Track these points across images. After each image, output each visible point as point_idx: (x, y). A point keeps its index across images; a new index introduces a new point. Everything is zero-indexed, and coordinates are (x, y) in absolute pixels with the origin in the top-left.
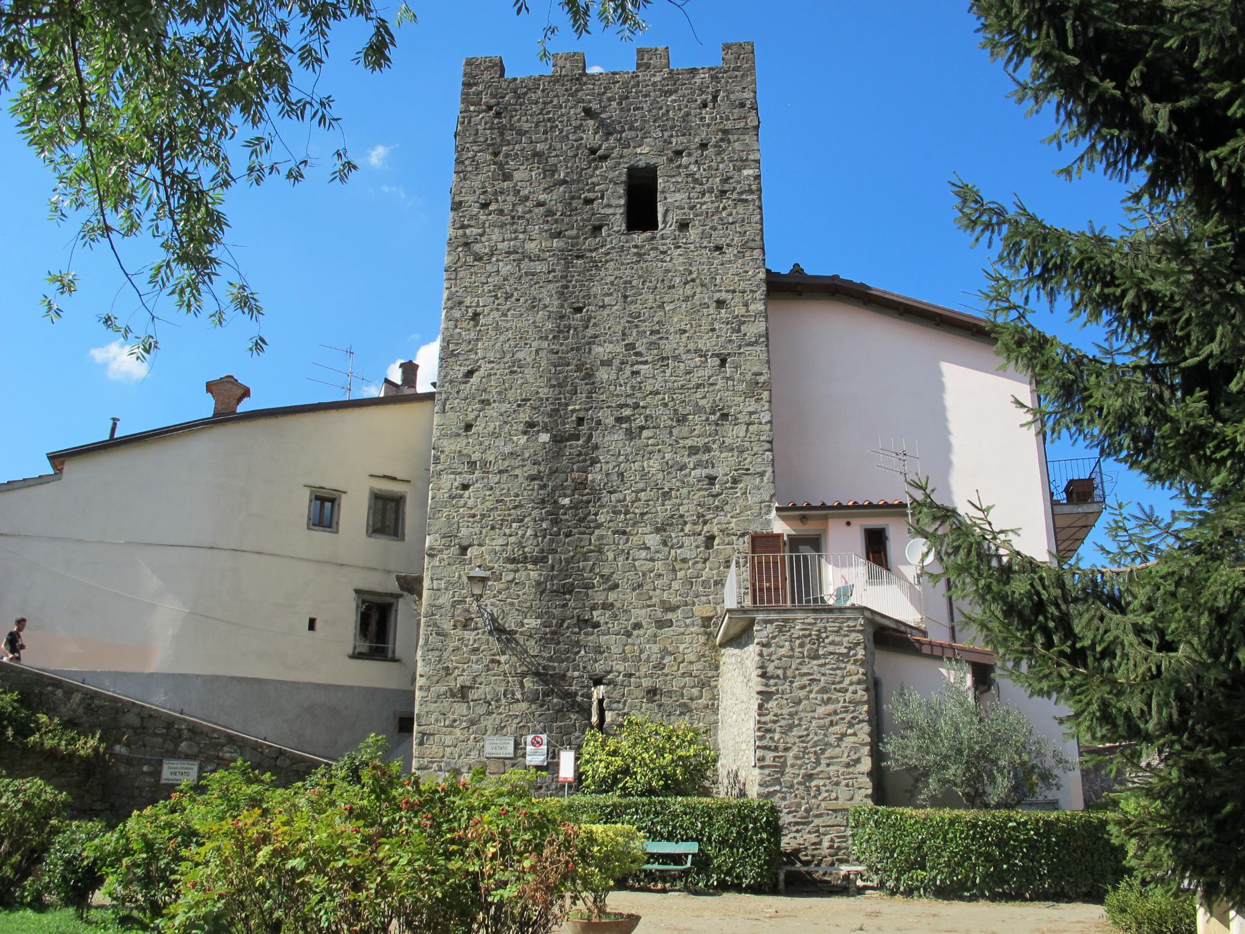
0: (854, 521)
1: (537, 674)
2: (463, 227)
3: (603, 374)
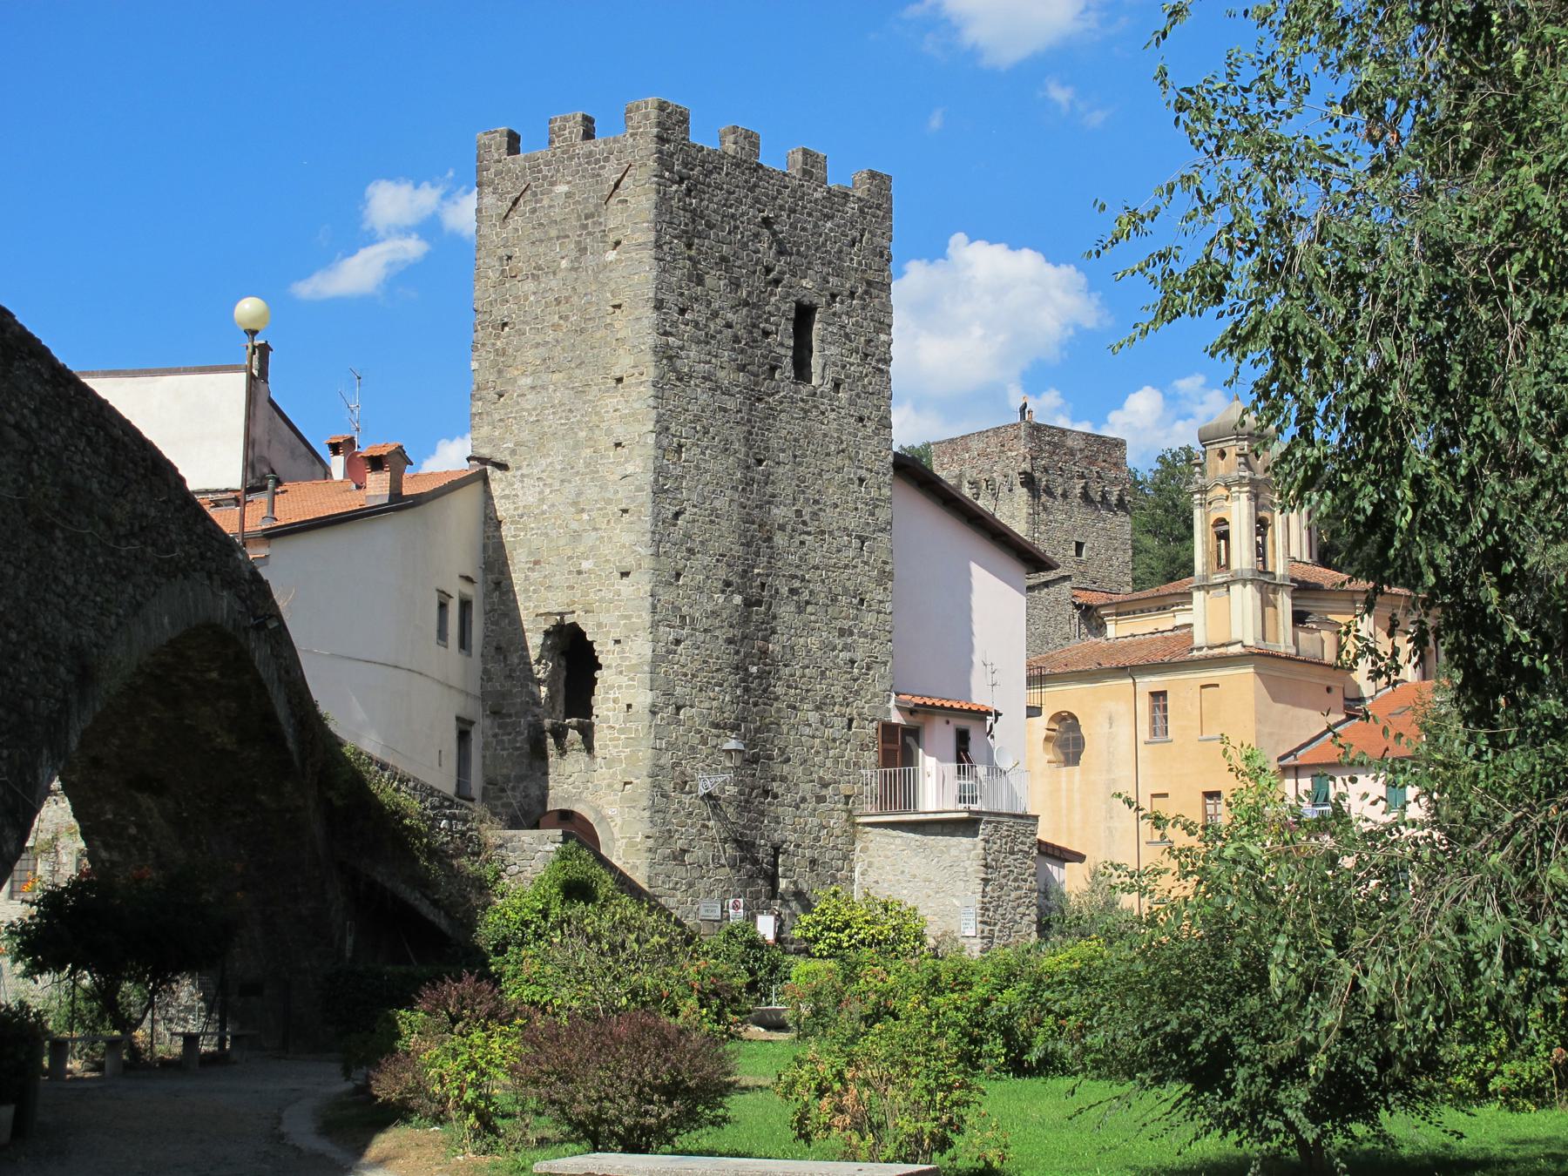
1: (736, 841)
2: (666, 334)
3: (780, 539)
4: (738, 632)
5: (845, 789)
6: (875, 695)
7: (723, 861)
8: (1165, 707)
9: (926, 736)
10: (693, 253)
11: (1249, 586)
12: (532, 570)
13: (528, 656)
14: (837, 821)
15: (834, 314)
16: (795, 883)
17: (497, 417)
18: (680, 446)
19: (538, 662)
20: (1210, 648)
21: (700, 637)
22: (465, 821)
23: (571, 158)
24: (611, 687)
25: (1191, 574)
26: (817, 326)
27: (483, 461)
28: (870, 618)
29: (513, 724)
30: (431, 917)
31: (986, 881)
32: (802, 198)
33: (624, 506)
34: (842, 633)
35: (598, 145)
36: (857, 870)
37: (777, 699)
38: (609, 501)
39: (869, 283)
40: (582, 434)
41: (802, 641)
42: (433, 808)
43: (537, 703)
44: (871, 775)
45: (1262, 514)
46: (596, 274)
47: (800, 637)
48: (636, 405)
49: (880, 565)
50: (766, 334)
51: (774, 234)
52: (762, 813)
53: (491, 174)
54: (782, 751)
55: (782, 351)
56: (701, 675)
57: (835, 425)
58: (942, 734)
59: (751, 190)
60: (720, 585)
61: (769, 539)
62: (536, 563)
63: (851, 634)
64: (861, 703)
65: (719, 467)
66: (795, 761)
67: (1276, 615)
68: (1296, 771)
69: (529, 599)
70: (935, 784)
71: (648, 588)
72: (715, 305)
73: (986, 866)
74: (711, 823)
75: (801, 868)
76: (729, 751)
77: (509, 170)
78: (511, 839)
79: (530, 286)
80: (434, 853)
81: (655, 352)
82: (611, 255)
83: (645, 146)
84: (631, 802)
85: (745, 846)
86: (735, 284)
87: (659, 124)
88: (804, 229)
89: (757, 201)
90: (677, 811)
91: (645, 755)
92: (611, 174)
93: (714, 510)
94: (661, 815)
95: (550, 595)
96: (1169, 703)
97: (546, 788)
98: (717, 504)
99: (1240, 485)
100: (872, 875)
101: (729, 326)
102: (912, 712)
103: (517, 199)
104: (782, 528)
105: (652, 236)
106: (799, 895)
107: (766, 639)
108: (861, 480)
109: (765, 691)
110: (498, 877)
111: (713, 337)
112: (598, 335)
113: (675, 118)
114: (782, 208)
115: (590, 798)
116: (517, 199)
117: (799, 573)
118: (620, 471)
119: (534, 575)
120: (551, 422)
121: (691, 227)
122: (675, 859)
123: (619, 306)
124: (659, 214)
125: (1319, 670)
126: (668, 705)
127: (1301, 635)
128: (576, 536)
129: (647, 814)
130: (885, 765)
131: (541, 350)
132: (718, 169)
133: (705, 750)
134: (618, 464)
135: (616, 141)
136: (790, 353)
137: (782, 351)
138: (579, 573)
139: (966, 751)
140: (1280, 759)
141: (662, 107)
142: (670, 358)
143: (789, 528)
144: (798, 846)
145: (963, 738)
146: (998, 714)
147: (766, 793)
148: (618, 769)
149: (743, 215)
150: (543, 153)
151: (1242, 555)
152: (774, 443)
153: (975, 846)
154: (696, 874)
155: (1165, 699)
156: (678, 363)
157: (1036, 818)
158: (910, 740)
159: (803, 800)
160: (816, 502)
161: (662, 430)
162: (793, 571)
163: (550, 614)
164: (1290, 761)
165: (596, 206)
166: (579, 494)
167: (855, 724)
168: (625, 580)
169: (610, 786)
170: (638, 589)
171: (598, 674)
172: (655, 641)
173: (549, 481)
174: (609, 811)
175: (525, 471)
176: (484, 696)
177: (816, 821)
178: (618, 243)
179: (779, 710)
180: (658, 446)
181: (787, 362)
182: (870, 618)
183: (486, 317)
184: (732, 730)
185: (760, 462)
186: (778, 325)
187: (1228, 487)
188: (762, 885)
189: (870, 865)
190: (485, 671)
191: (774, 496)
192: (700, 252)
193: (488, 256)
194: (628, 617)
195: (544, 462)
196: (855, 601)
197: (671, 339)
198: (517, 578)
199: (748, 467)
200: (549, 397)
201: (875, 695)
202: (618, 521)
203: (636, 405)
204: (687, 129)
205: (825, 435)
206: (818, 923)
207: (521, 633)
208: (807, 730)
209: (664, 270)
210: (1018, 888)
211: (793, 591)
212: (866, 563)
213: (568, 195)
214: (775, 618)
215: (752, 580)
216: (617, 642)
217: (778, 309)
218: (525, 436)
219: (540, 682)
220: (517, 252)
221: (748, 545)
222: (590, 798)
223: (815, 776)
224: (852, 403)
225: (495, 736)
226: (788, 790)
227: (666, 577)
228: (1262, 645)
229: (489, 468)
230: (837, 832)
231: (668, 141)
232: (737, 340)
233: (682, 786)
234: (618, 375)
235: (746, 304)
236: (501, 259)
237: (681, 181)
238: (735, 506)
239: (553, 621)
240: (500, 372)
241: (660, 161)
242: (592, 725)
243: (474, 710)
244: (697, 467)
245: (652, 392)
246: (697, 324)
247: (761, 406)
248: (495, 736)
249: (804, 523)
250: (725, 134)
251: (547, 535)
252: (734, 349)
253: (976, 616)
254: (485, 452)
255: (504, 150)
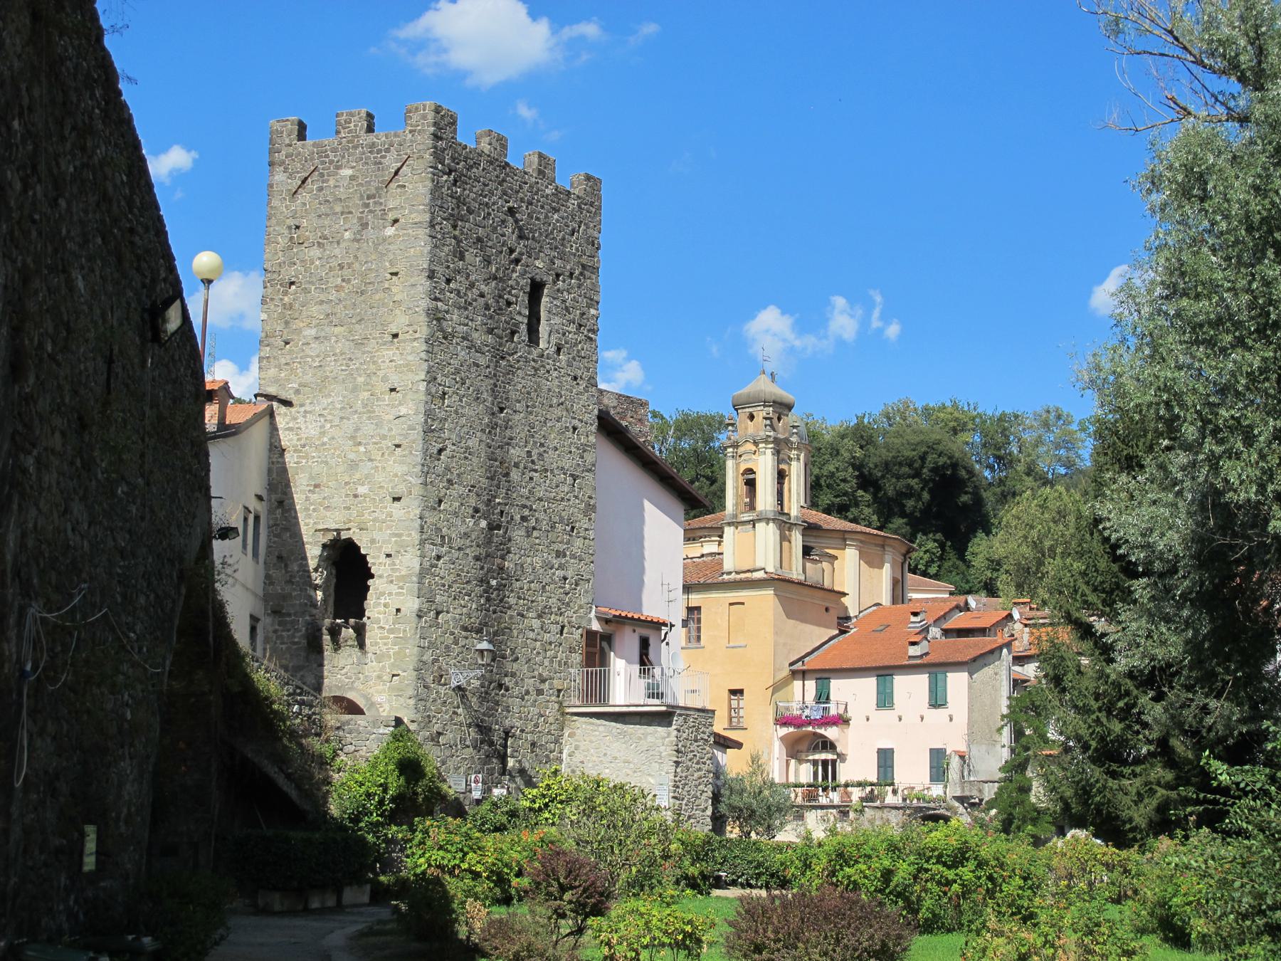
0: (638, 630)
1: (478, 726)
2: (436, 299)
3: (515, 475)
4: (483, 551)
5: (557, 684)
6: (581, 607)
7: (468, 743)
8: (699, 620)
9: (617, 642)
10: (457, 233)
11: (771, 524)
12: (313, 492)
13: (307, 565)
14: (552, 711)
15: (558, 290)
16: (520, 762)
17: (283, 361)
18: (444, 394)
19: (316, 570)
20: (737, 573)
21: (455, 554)
22: (311, 706)
23: (355, 147)
24: (383, 594)
25: (723, 507)
26: (544, 299)
27: (270, 398)
28: (578, 543)
29: (292, 622)
30: (285, 788)
31: (677, 763)
32: (537, 193)
33: (397, 442)
34: (559, 554)
35: (379, 137)
36: (565, 752)
37: (510, 608)
38: (384, 437)
39: (584, 266)
40: (361, 380)
41: (529, 560)
42: (289, 695)
43: (314, 605)
44: (576, 673)
45: (782, 466)
46: (376, 245)
47: (528, 556)
48: (410, 358)
49: (586, 499)
50: (509, 304)
51: (517, 221)
52: (497, 703)
53: (282, 156)
54: (513, 651)
55: (519, 318)
56: (455, 586)
57: (556, 382)
58: (629, 641)
59: (500, 184)
60: (471, 511)
61: (507, 475)
62: (316, 486)
63: (565, 556)
64: (570, 613)
65: (471, 413)
66: (522, 660)
67: (791, 548)
68: (803, 674)
69: (309, 516)
70: (624, 684)
71: (418, 512)
72: (473, 278)
73: (678, 751)
74: (460, 711)
75: (525, 749)
76: (482, 651)
77: (299, 153)
78: (348, 723)
79: (315, 252)
80: (293, 734)
81: (428, 315)
82: (390, 231)
83: (424, 141)
84: (398, 692)
85: (484, 729)
86: (487, 261)
87: (435, 124)
88: (538, 219)
89: (505, 193)
90: (435, 700)
91: (411, 651)
92: (391, 162)
93: (467, 448)
94: (423, 703)
95: (328, 514)
96: (703, 616)
97: (322, 677)
98: (470, 443)
99: (766, 442)
100: (578, 757)
101: (482, 295)
102: (607, 621)
103: (306, 179)
104: (516, 465)
105: (427, 217)
106: (522, 772)
107: (503, 558)
108: (575, 429)
109: (501, 601)
110: (335, 755)
111: (470, 304)
112: (377, 297)
113: (447, 120)
114: (522, 200)
115: (361, 687)
116: (306, 179)
117: (529, 504)
118: (394, 412)
119: (314, 497)
120: (332, 367)
121: (456, 212)
122: (433, 740)
123: (396, 274)
124: (433, 199)
125: (821, 593)
126: (430, 611)
127: (808, 565)
128: (353, 465)
129: (412, 702)
130: (588, 666)
131: (324, 306)
132: (477, 164)
133: (457, 649)
134: (393, 406)
135: (396, 135)
136: (526, 321)
137: (519, 318)
138: (356, 496)
139: (647, 655)
140: (791, 664)
141: (437, 110)
142: (438, 320)
143: (522, 466)
144: (522, 731)
145: (644, 644)
146: (672, 626)
147: (500, 686)
148: (387, 663)
149: (494, 204)
150: (329, 141)
151: (765, 499)
152: (513, 395)
153: (669, 735)
154: (448, 753)
155: (699, 613)
156: (444, 324)
157: (713, 712)
158: (605, 644)
159: (527, 693)
160: (542, 445)
161: (432, 380)
162: (524, 502)
163: (327, 530)
164: (799, 666)
165: (377, 189)
166: (357, 429)
167: (566, 630)
168: (397, 504)
169: (379, 677)
170: (410, 510)
171: (370, 582)
172: (423, 556)
173: (329, 417)
174: (377, 699)
175: (308, 408)
176: (266, 598)
177: (536, 710)
178: (396, 221)
179: (511, 617)
180: (428, 393)
181: (523, 327)
182: (578, 543)
183: (275, 276)
184: (477, 633)
185: (502, 410)
186: (517, 297)
187: (756, 443)
188: (495, 763)
189: (577, 748)
190: (267, 577)
191: (511, 439)
192: (462, 233)
193: (278, 224)
194: (399, 535)
195: (325, 401)
196: (568, 528)
197: (440, 304)
198: (299, 499)
199: (493, 414)
200: (332, 347)
201: (581, 607)
202: (392, 453)
203: (410, 358)
204: (455, 130)
205: (549, 390)
206: (544, 796)
207: (300, 544)
208: (532, 635)
209: (436, 246)
210: (700, 770)
211: (524, 519)
212: (576, 497)
213: (352, 178)
214: (510, 540)
215: (494, 508)
216: (388, 556)
217: (518, 283)
218: (308, 378)
219: (316, 587)
220: (304, 223)
221: (492, 478)
222: (361, 687)
223: (536, 673)
224: (569, 365)
225: (275, 631)
226: (516, 683)
227: (432, 503)
228: (779, 572)
229: (275, 404)
230: (551, 720)
231: (441, 139)
232: (487, 307)
233: (439, 679)
234: (395, 331)
235: (495, 278)
236: (289, 228)
237: (449, 174)
238: (483, 446)
239: (331, 536)
240: (287, 323)
241: (435, 154)
242: (364, 625)
243: (259, 613)
244: (456, 412)
245: (424, 347)
246: (459, 292)
247: (503, 363)
248: (275, 631)
249: (533, 462)
250: (481, 136)
251: (326, 463)
252: (485, 315)
253: (647, 544)
254: (272, 390)
255: (294, 136)
